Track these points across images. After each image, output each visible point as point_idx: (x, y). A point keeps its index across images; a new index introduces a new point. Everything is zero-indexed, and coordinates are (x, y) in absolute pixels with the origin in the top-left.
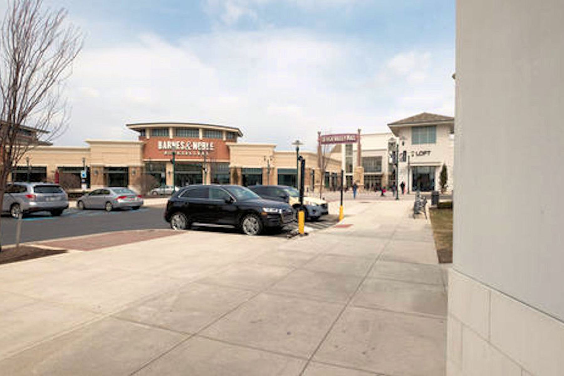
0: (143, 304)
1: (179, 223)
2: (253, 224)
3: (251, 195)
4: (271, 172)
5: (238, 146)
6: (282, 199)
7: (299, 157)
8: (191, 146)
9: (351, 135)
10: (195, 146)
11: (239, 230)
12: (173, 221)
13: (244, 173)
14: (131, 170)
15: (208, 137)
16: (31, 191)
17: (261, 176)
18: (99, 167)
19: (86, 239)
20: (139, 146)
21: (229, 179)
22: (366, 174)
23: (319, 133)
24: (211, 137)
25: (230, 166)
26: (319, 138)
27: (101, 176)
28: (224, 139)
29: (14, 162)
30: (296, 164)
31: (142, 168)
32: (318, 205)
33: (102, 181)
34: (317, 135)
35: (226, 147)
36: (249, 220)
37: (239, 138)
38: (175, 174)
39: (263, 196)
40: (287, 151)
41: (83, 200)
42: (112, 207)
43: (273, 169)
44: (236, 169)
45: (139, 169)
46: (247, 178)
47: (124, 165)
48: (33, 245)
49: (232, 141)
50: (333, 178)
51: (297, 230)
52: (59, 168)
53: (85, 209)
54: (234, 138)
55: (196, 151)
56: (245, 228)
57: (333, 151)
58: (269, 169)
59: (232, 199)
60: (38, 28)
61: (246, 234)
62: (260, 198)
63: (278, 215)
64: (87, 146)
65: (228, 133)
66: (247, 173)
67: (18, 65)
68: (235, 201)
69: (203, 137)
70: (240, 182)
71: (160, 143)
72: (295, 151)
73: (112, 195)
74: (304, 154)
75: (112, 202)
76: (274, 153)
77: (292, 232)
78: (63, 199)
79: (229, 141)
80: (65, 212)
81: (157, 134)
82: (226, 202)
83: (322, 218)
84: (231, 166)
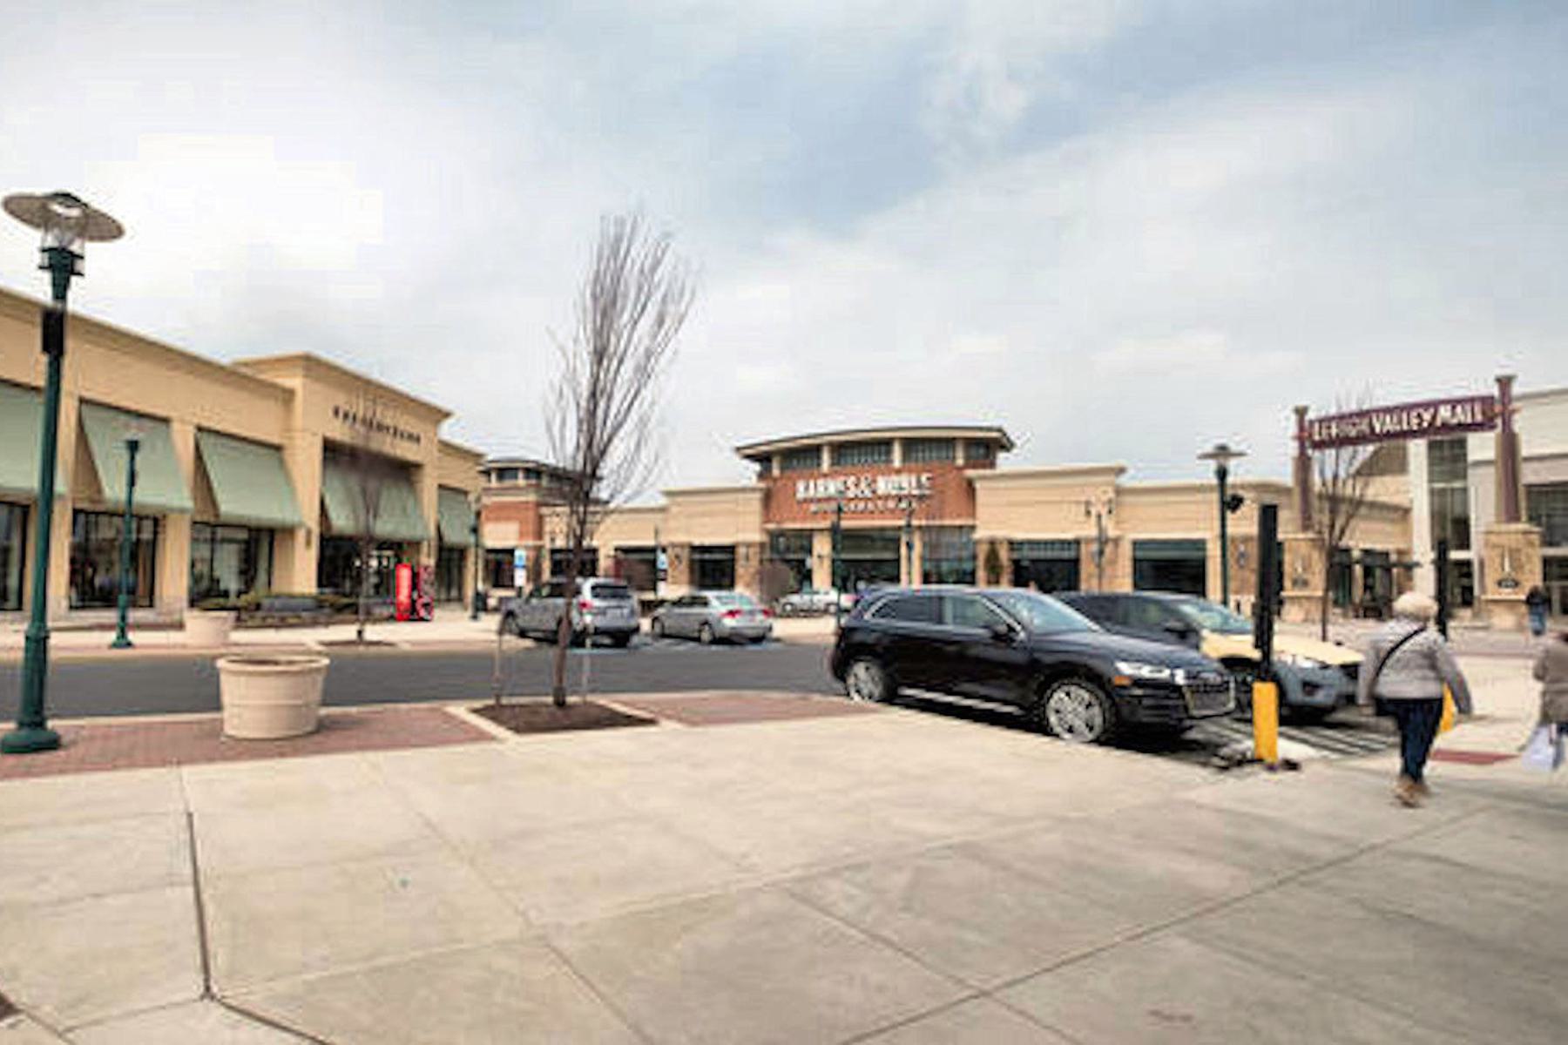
0: (835, 873)
1: (866, 683)
2: (1081, 709)
3: (1064, 617)
4: (1108, 549)
5: (1004, 476)
6: (1173, 637)
7: (1228, 498)
8: (873, 486)
9: (1454, 403)
10: (884, 485)
11: (1033, 722)
12: (851, 680)
13: (1016, 556)
14: (741, 551)
15: (924, 458)
16: (587, 595)
17: (1076, 562)
18: (682, 546)
19: (682, 700)
20: (758, 495)
21: (973, 573)
22: (1551, 552)
23: (1301, 412)
24: (931, 457)
25: (977, 535)
26: (1301, 428)
27: (684, 566)
28: (960, 462)
29: (588, 539)
30: (1217, 524)
31: (762, 545)
32: (1325, 667)
33: (685, 577)
34: (1294, 418)
35: (965, 485)
36: (1068, 694)
37: (1001, 456)
38: (833, 561)
39: (1108, 625)
40: (1198, 482)
41: (663, 618)
42: (713, 634)
43: (1116, 541)
44: (993, 543)
45: (757, 549)
46: (1026, 568)
47: (1069, 536)
48: (602, 700)
49: (984, 466)
50: (1368, 572)
51: (1248, 744)
52: (616, 549)
53: (664, 636)
54: (987, 456)
55: (887, 497)
56: (1053, 719)
57: (1369, 470)
58: (1103, 540)
59: (1011, 629)
60: (631, 276)
61: (1057, 736)
62: (1102, 631)
63: (1170, 687)
64: (663, 501)
65: (971, 443)
66: (1027, 554)
67: (600, 355)
68: (1022, 635)
69: (833, 464)
70: (1006, 577)
71: (801, 486)
72: (1214, 481)
73: (714, 607)
74: (1243, 487)
75: (714, 623)
76: (1119, 491)
77: (1225, 751)
78: (632, 613)
79: (974, 467)
80: (635, 640)
81: (856, 460)
82: (997, 637)
83: (1341, 716)
84: (980, 534)
